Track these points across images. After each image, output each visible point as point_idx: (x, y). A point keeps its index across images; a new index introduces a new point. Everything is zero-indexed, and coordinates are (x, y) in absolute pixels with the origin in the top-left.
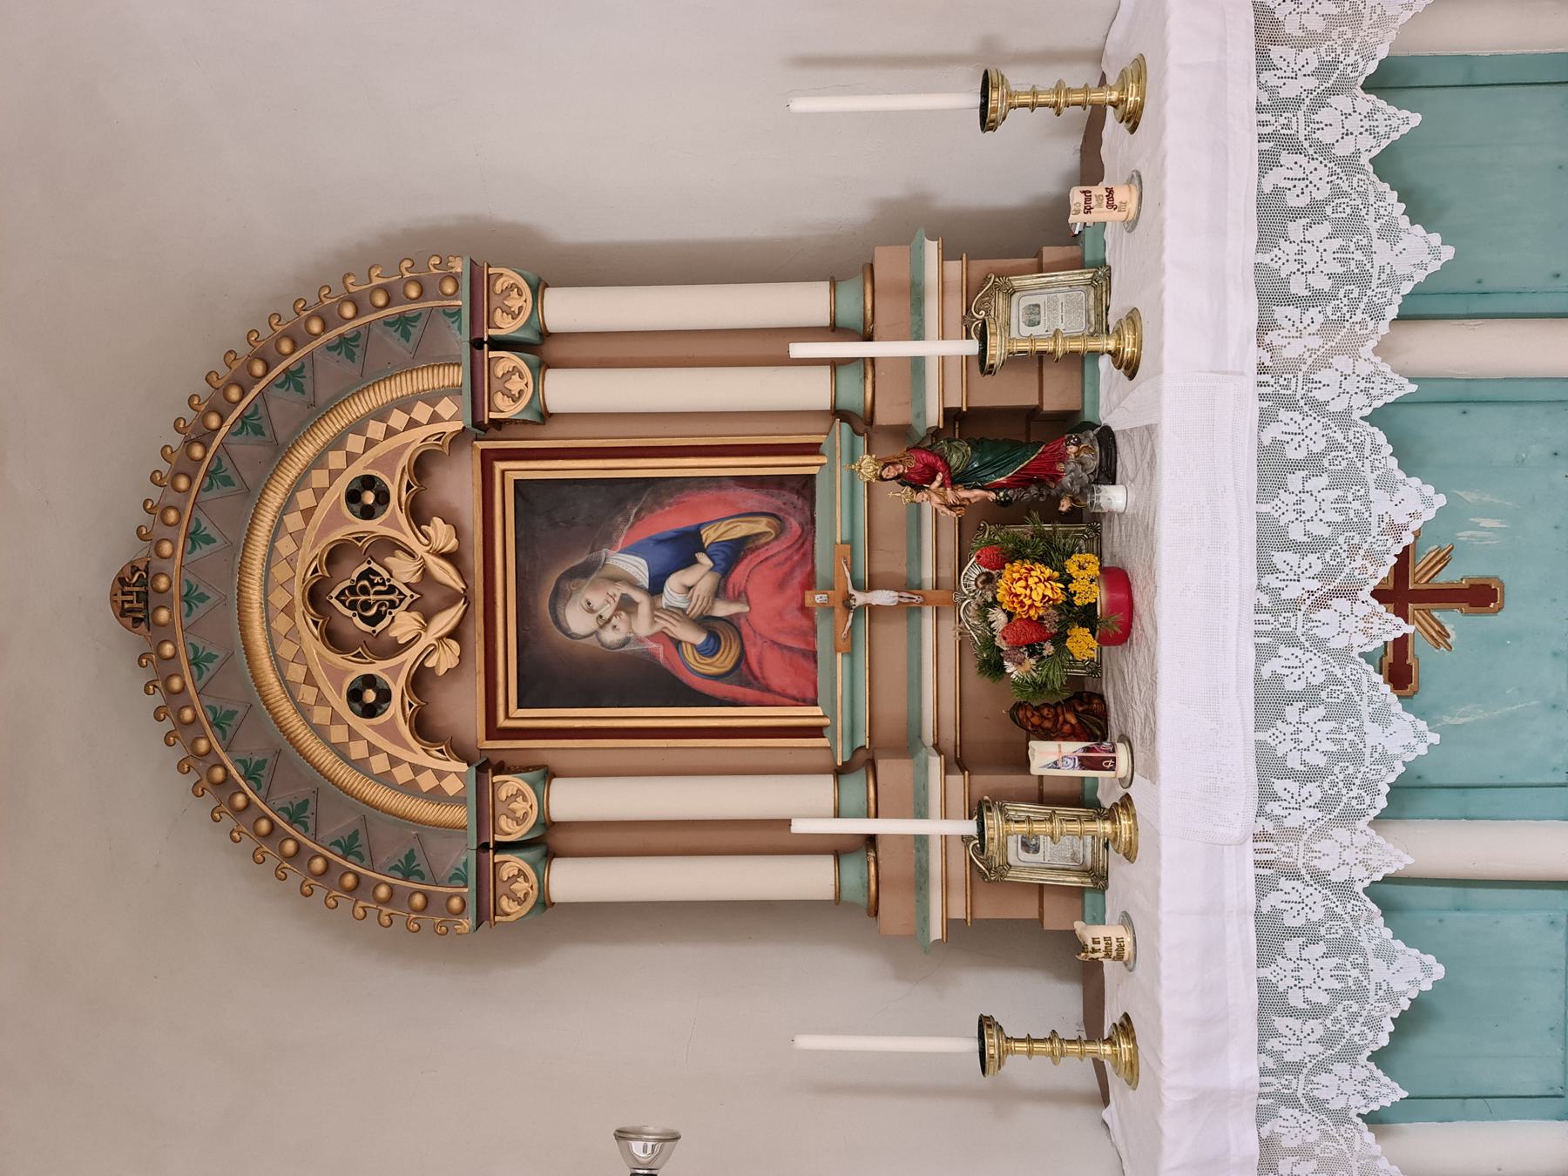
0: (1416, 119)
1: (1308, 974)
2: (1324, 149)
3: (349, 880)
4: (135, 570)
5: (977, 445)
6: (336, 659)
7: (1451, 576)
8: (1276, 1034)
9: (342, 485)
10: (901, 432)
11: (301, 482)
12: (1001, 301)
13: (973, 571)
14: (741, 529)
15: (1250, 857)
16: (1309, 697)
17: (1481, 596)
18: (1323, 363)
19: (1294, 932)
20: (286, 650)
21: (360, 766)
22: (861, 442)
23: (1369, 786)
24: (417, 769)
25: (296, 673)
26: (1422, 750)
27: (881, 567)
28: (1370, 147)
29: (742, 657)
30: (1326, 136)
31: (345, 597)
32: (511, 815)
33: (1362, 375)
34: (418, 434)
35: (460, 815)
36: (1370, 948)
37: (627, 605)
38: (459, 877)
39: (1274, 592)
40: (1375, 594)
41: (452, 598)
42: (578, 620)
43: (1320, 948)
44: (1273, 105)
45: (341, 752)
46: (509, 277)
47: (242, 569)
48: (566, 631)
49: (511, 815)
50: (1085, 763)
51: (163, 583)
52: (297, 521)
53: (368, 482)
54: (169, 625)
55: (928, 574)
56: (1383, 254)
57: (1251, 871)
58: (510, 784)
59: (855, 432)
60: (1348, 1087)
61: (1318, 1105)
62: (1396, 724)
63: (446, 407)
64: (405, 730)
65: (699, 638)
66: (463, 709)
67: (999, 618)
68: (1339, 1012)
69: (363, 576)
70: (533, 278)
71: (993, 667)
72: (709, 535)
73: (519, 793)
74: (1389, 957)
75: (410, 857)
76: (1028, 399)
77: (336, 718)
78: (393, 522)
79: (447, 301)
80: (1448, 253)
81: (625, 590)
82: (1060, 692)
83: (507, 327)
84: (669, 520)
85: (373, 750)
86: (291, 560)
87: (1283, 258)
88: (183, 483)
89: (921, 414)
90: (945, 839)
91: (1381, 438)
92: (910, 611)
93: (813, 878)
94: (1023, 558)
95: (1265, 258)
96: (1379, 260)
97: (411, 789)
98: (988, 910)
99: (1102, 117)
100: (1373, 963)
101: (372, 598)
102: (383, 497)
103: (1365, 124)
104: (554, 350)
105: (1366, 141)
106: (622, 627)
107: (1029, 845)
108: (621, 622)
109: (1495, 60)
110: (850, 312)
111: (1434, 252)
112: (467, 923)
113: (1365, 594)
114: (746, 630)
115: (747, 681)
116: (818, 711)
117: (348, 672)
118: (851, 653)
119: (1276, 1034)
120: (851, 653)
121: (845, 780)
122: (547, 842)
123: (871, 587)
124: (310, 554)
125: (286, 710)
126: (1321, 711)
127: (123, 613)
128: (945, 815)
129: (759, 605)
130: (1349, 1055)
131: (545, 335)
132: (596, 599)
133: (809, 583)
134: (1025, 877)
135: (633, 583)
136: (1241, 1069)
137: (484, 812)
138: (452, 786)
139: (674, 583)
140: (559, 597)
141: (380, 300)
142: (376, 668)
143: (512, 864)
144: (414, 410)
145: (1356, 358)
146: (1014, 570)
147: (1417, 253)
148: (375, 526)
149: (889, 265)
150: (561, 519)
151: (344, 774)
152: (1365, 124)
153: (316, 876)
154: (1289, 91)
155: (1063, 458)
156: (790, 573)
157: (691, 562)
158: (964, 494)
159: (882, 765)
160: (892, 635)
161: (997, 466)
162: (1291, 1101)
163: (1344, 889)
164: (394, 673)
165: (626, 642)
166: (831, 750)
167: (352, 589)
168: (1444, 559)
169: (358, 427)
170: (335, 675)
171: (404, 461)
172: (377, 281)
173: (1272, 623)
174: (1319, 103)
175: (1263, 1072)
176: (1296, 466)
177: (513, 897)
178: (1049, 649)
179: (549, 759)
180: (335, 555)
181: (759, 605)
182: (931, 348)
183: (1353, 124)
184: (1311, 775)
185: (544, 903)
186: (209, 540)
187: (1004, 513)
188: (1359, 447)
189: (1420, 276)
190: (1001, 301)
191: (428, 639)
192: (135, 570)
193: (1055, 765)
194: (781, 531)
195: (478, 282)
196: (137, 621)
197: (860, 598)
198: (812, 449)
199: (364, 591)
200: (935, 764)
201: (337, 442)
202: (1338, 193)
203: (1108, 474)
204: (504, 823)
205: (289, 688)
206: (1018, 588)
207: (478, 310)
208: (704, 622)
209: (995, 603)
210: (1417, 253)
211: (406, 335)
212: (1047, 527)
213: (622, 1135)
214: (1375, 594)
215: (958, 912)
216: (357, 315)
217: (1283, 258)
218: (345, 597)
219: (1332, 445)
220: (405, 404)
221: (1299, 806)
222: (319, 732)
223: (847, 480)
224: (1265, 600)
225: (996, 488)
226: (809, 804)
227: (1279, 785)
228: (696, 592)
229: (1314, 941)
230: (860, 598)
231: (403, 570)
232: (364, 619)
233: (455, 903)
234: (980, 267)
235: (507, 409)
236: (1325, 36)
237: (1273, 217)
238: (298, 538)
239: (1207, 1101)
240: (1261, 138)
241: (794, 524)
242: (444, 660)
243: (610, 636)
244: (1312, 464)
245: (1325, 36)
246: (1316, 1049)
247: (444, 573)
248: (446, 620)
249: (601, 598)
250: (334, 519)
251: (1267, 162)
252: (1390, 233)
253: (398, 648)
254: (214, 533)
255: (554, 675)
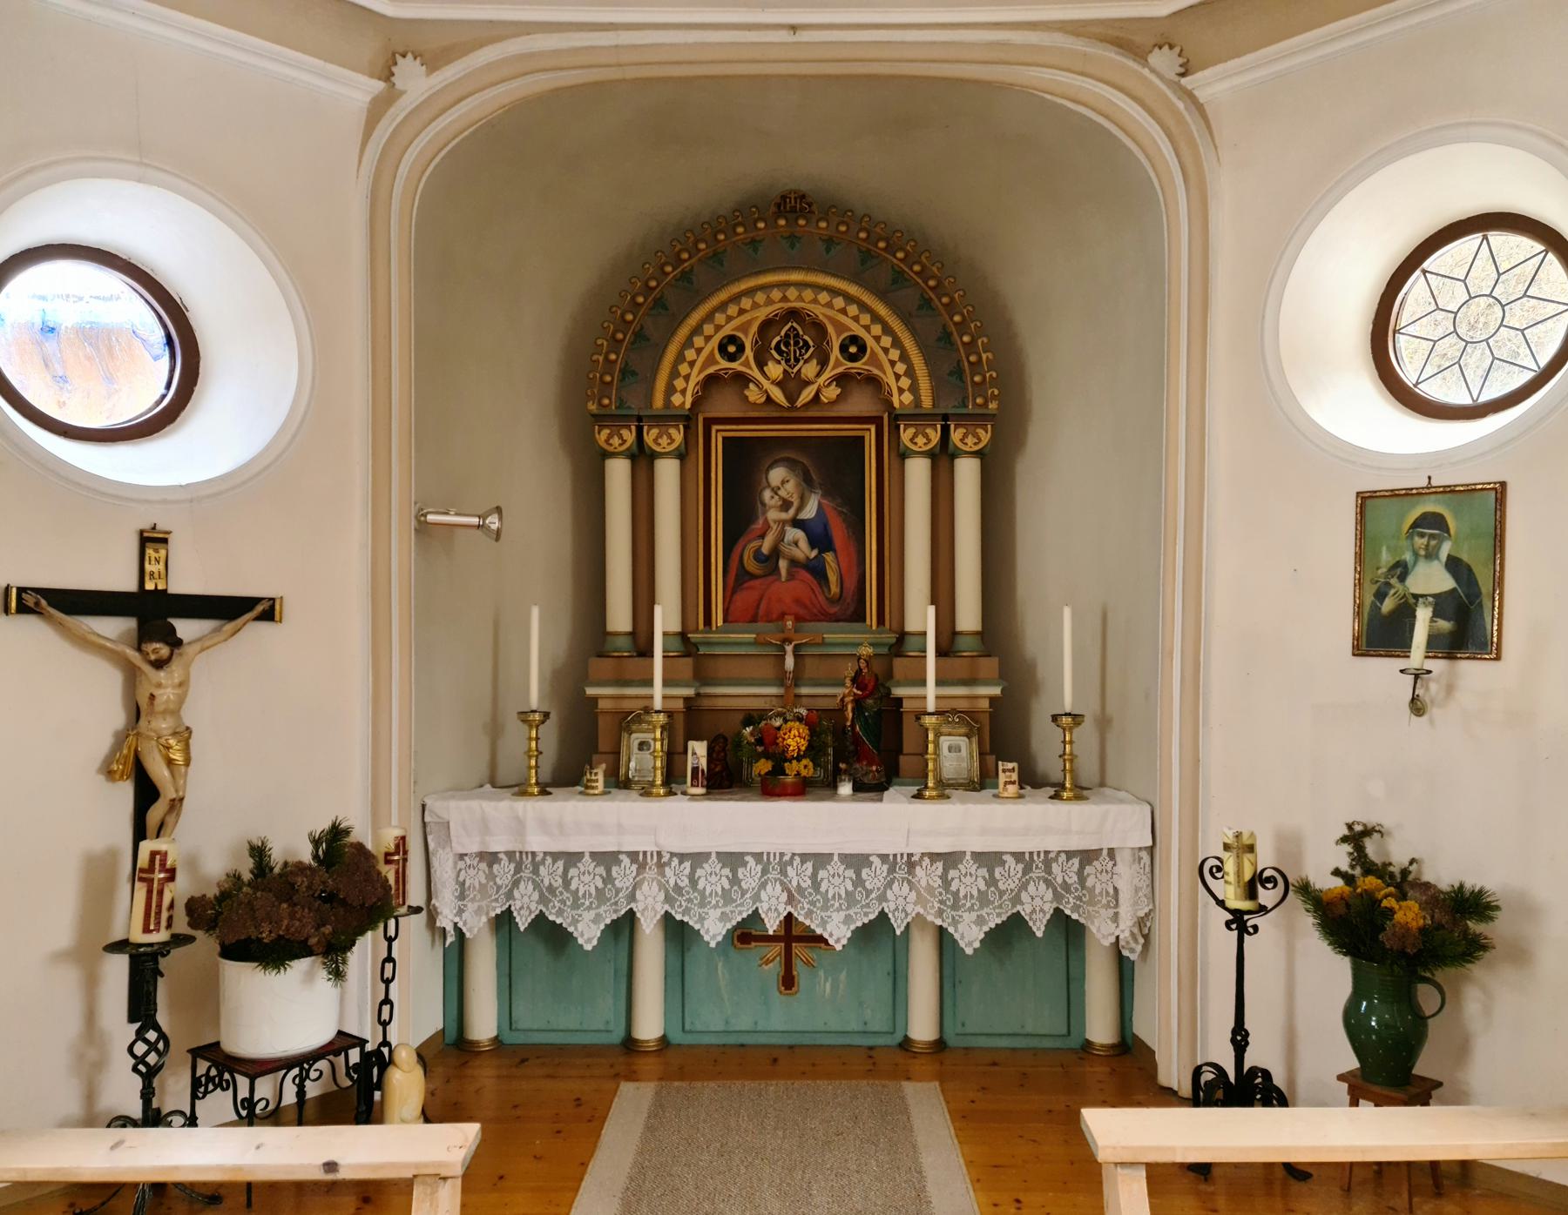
0: (1039, 934)
1: (587, 878)
2: (1024, 887)
3: (620, 336)
4: (810, 205)
5: (879, 713)
6: (754, 328)
7: (799, 969)
8: (554, 862)
9: (862, 333)
10: (889, 674)
11: (864, 307)
12: (963, 730)
13: (804, 712)
14: (833, 578)
15: (648, 849)
16: (735, 880)
17: (788, 981)
18: (912, 886)
19: (609, 871)
20: (760, 297)
21: (688, 343)
22: (885, 650)
23: (687, 911)
24: (687, 378)
25: (746, 303)
26: (706, 938)
27: (808, 661)
28: (1025, 910)
29: (753, 577)
30: (1031, 887)
31: (792, 334)
32: (660, 436)
33: (902, 905)
34: (891, 380)
35: (658, 402)
36: (601, 910)
37: (786, 505)
38: (621, 404)
39: (791, 862)
40: (790, 914)
41: (791, 398)
42: (777, 475)
43: (600, 885)
44: (1048, 859)
45: (697, 331)
46: (985, 437)
47: (809, 269)
48: (771, 467)
49: (660, 436)
50: (695, 770)
51: (802, 222)
52: (838, 304)
53: (862, 348)
54: (777, 226)
55: (804, 691)
56: (969, 917)
57: (641, 849)
58: (678, 436)
59: (891, 646)
60: (526, 899)
61: (516, 884)
62: (721, 925)
63: (907, 398)
64: (711, 370)
65: (765, 549)
66: (723, 404)
67: (778, 722)
68: (566, 895)
69: (806, 343)
70: (986, 451)
71: (746, 723)
72: (829, 557)
73: (673, 441)
74: (596, 920)
75: (634, 373)
76: (907, 748)
77: (718, 328)
78: (837, 363)
79: (981, 391)
80: (969, 951)
81: (796, 504)
82: (737, 764)
83: (956, 436)
84: (839, 532)
85: (699, 351)
86: (815, 301)
87: (968, 865)
88: (863, 235)
89: (899, 684)
90: (651, 697)
91: (872, 917)
92: (780, 680)
93: (620, 618)
94: (811, 735)
95: (968, 857)
96: (966, 915)
97: (674, 374)
98: (603, 723)
99: (1006, 746)
100: (593, 913)
101: (792, 350)
102: (853, 358)
103: (1037, 909)
104: (943, 462)
105: (1028, 908)
106: (773, 502)
107: (643, 746)
108: (776, 501)
109: (1083, 993)
110: (962, 643)
111: (970, 944)
112: (592, 407)
113: (789, 909)
114: (770, 579)
115: (738, 579)
116: (720, 623)
117: (746, 335)
118: (756, 643)
119: (554, 862)
120: (756, 643)
121: (678, 639)
122: (643, 459)
123: (797, 656)
124: (819, 312)
125: (723, 295)
126: (727, 886)
127: (784, 197)
128: (664, 697)
129: (786, 588)
130: (543, 900)
131: (953, 457)
132: (790, 486)
133: (798, 619)
134: (624, 743)
135: (800, 509)
136: (537, 843)
137: (665, 419)
138: (677, 399)
139: (799, 534)
140: (791, 464)
141: (973, 358)
142: (749, 353)
143: (629, 436)
144: (905, 379)
145: (915, 904)
146: (804, 730)
147: (969, 936)
148: (835, 353)
149: (989, 666)
150: (838, 467)
151: (683, 332)
152: (1037, 909)
153: (622, 316)
154: (1055, 868)
155: (870, 764)
156: (806, 607)
157: (812, 545)
158: (850, 707)
159: (689, 660)
160: (766, 669)
161: (865, 728)
162: (518, 870)
163: (632, 897)
164: (746, 364)
165: (763, 504)
166: (697, 631)
167: (797, 335)
168: (808, 963)
169: (897, 343)
170: (744, 328)
171: (876, 371)
172: (984, 356)
173: (774, 862)
174: (1048, 883)
175: (533, 854)
176: (858, 874)
177: (610, 436)
178: (760, 749)
179: (693, 456)
180: (819, 329)
181: (786, 588)
182: (931, 690)
183: (1038, 901)
184: (693, 882)
185: (606, 455)
186: (828, 250)
187: (840, 732)
188: (868, 905)
189: (957, 936)
190: (963, 730)
191: (766, 384)
192: (810, 205)
193: (694, 754)
194: (832, 601)
195: (981, 418)
196: (779, 205)
197: (789, 648)
198: (881, 620)
199: (796, 343)
200: (690, 692)
201: (887, 330)
202: (1002, 893)
203: (858, 788)
204: (655, 432)
205: (735, 299)
206: (794, 732)
207: (965, 419)
208: (776, 553)
209: (786, 721)
210: (969, 936)
211: (951, 374)
212: (830, 751)
213: (499, 510)
214: (790, 914)
215: (602, 704)
216: (964, 344)
217: (968, 865)
218: (792, 334)
219: (869, 892)
220: (910, 373)
221: (677, 874)
222: (709, 317)
223: (861, 641)
224: (787, 858)
225: (853, 726)
226: (666, 618)
227: (687, 864)
228: (794, 549)
229: (604, 881)
230: (789, 648)
231: (809, 370)
232: (778, 343)
233: (606, 401)
234: (986, 720)
235: (906, 435)
236: (1083, 887)
237: (988, 860)
238: (829, 305)
239: (519, 826)
240: (1031, 853)
241: (833, 610)
242: (753, 394)
243: (767, 494)
244: (858, 882)
245: (1083, 887)
246: (546, 883)
247: (807, 395)
248: (777, 395)
249: (790, 489)
250: (840, 327)
251: (1018, 856)
252: (980, 921)
253: (761, 365)
254: (833, 252)
255: (745, 463)
